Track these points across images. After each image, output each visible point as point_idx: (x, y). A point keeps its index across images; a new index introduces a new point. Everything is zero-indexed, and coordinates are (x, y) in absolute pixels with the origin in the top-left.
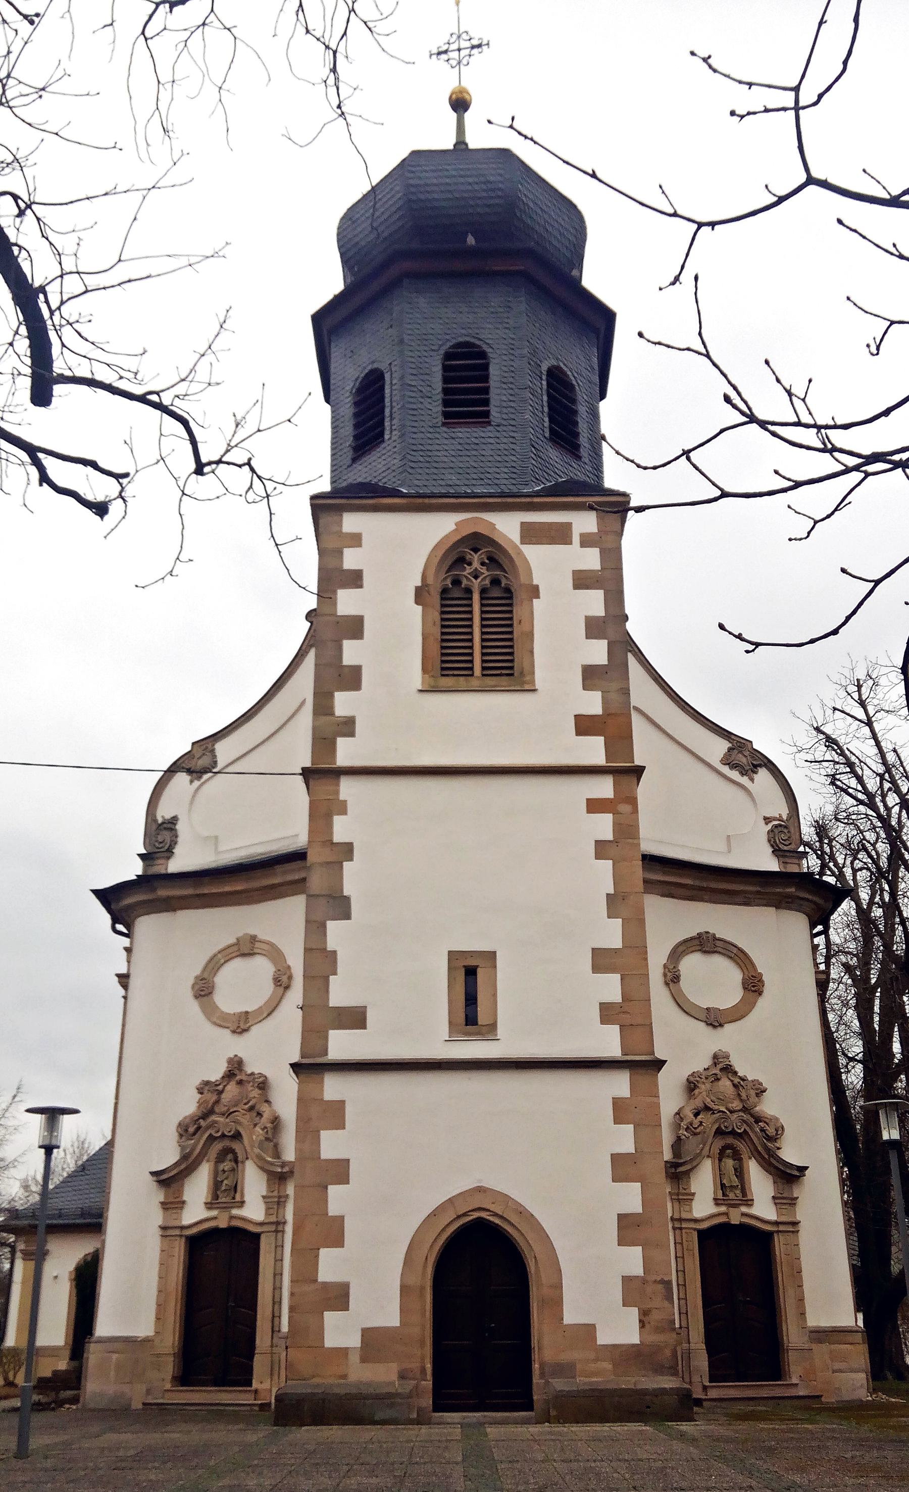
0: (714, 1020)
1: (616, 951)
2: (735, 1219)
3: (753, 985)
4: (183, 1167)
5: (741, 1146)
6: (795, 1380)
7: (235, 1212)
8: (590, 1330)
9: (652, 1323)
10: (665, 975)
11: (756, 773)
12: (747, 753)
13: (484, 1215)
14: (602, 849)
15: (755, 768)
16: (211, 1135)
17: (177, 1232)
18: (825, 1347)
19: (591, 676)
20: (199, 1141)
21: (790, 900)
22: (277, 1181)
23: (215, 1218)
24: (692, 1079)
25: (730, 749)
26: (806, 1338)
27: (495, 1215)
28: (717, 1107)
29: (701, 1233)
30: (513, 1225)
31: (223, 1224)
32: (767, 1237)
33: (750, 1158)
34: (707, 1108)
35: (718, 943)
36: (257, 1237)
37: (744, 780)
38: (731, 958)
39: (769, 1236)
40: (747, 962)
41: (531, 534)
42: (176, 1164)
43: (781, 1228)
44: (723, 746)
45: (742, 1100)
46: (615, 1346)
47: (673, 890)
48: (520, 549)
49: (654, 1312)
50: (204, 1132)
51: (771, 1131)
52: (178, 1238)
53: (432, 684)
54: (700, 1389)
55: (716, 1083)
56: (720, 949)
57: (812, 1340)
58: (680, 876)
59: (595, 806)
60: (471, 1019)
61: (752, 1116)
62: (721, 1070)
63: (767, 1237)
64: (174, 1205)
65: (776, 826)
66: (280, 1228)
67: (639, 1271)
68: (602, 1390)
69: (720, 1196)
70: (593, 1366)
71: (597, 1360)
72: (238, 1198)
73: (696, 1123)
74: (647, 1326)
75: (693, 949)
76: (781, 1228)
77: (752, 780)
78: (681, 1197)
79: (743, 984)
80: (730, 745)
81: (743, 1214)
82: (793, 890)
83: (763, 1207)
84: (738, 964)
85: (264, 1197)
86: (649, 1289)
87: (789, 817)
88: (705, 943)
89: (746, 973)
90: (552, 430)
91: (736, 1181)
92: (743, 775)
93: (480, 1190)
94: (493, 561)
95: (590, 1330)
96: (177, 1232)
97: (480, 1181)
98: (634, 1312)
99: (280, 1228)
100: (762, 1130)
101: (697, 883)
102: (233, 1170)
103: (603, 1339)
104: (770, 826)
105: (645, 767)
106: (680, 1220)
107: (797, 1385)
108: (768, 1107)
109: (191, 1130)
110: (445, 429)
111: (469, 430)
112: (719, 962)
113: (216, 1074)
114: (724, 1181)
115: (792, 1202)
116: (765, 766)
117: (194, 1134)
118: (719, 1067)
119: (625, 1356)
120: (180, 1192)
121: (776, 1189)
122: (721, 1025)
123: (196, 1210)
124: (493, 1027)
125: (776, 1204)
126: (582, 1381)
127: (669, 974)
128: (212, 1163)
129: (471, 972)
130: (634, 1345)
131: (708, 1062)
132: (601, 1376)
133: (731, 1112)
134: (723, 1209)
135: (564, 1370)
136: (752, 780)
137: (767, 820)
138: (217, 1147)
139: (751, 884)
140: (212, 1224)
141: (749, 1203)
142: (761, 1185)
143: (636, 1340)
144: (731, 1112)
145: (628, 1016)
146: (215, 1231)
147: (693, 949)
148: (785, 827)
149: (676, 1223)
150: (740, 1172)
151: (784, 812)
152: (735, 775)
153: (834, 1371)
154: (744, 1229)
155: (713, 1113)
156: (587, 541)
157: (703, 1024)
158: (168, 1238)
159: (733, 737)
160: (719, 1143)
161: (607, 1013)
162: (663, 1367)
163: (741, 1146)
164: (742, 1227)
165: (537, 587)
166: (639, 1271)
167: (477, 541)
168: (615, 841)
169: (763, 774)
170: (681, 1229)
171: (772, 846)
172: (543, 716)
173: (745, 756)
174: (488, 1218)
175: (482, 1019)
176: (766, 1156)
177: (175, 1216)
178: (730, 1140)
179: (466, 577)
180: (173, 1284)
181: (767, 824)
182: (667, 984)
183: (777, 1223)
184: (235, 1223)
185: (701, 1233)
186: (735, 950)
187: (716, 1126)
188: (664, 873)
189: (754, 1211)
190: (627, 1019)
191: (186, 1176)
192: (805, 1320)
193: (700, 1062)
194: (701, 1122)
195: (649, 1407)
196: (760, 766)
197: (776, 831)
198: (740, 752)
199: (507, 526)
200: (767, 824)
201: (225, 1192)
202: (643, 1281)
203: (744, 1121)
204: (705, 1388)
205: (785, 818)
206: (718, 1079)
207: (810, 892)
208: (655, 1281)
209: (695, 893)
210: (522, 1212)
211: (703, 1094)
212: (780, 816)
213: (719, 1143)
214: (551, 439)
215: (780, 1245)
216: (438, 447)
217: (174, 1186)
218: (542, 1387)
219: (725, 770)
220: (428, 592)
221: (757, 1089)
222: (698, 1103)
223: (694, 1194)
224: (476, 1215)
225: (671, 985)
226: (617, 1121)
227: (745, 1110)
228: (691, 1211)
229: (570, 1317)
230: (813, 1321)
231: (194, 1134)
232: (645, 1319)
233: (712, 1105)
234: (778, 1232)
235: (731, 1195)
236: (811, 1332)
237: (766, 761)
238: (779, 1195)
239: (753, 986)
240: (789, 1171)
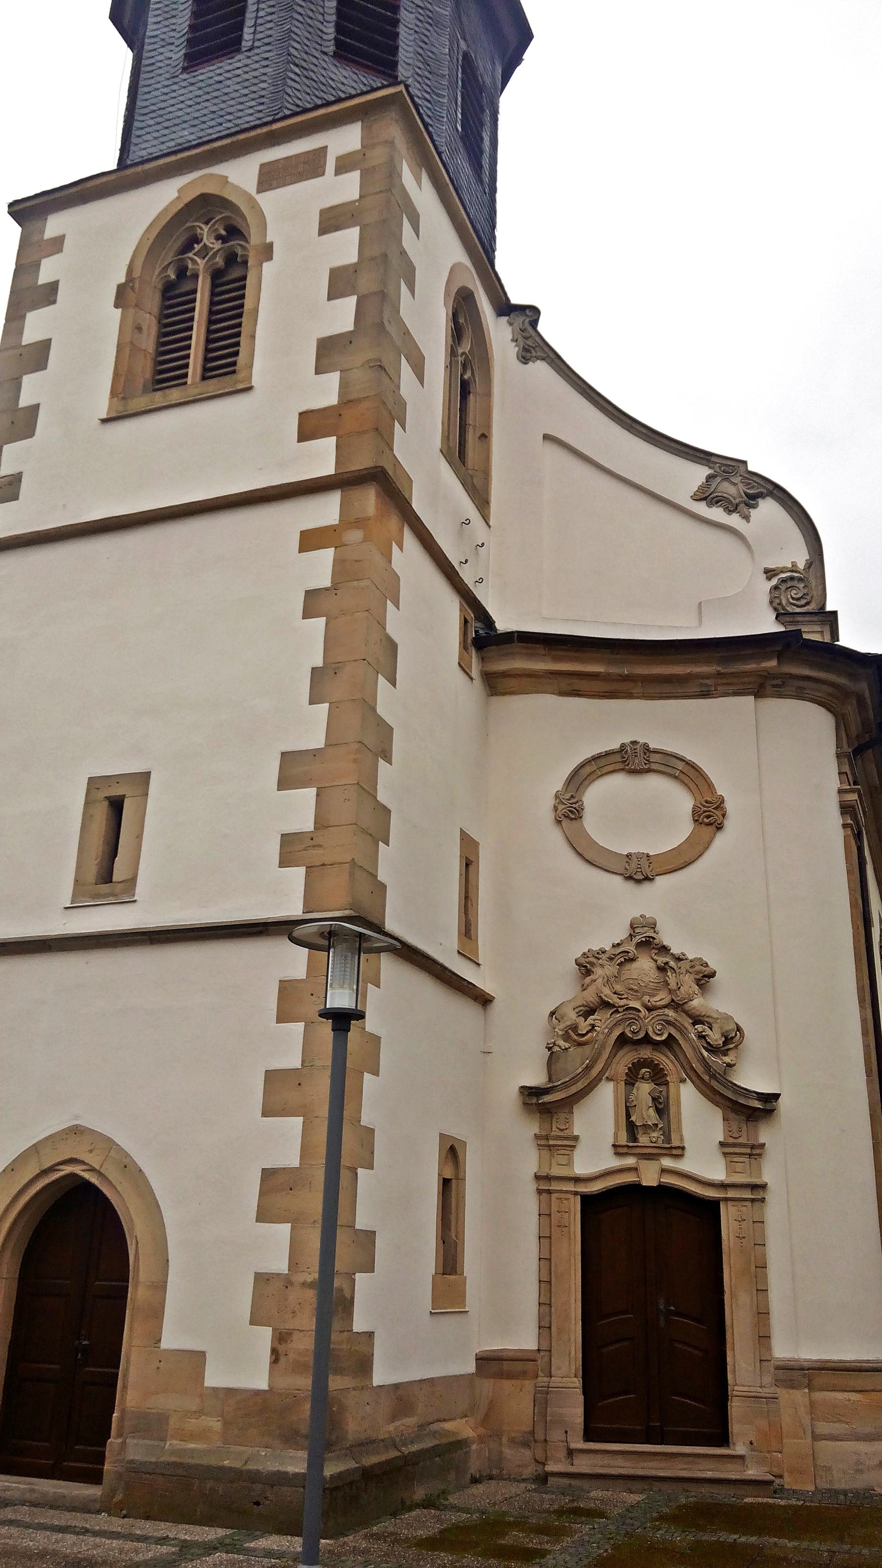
0: (639, 871)
1: (315, 753)
2: (649, 1177)
3: (710, 816)
5: (666, 1061)
6: (740, 1449)
8: (196, 1360)
9: (292, 1356)
10: (556, 809)
11: (754, 507)
12: (737, 480)
13: (77, 1169)
14: (313, 603)
15: (752, 500)
16: (623, 1034)
18: (800, 1396)
19: (329, 352)
21: (779, 682)
24: (583, 961)
25: (709, 478)
26: (768, 1379)
27: (92, 1170)
28: (622, 1003)
29: (587, 1200)
30: (110, 1183)
32: (708, 1210)
33: (683, 1081)
34: (605, 1005)
35: (654, 758)
37: (734, 520)
38: (676, 778)
39: (711, 1208)
40: (700, 781)
41: (270, 178)
43: (731, 1194)
44: (699, 473)
45: (670, 991)
46: (230, 1392)
47: (584, 685)
48: (255, 200)
49: (296, 1336)
51: (715, 1037)
53: (121, 408)
54: (562, 1454)
55: (628, 966)
56: (654, 766)
57: (778, 1382)
58: (582, 661)
59: (310, 540)
60: (106, 876)
61: (687, 1013)
62: (639, 945)
63: (708, 1210)
64: (557, 1144)
65: (784, 581)
67: (282, 1266)
68: (189, 1467)
69: (623, 1139)
70: (192, 1424)
71: (199, 1413)
73: (583, 1026)
74: (283, 1360)
75: (611, 768)
76: (731, 1194)
77: (747, 518)
78: (551, 1142)
79: (694, 812)
80: (710, 471)
81: (664, 1171)
82: (773, 663)
83: (701, 1155)
84: (683, 782)
86: (294, 1296)
87: (809, 565)
88: (634, 760)
89: (699, 797)
90: (338, 43)
91: (652, 1116)
92: (730, 512)
93: (76, 1131)
94: (234, 232)
95: (196, 1360)
96: (570, 1187)
97: (77, 1117)
98: (265, 1335)
100: (701, 1037)
101: (614, 670)
103: (213, 1378)
104: (774, 581)
105: (298, 442)
106: (548, 1178)
107: (742, 1457)
108: (722, 1003)
110: (185, 76)
111: (211, 68)
112: (656, 784)
114: (633, 1118)
115: (756, 1152)
116: (770, 494)
118: (637, 939)
119: (249, 1411)
120: (569, 1121)
121: (728, 1131)
122: (648, 879)
123: (596, 1151)
124: (131, 882)
125: (725, 1154)
126: (173, 1449)
127: (561, 807)
129: (116, 806)
130: (257, 1393)
131: (621, 933)
132: (199, 1441)
133: (649, 1009)
134: (630, 1161)
135: (152, 1425)
136: (747, 518)
137: (770, 573)
139: (708, 662)
141: (678, 1152)
142: (699, 1123)
143: (262, 1384)
144: (649, 1009)
145: (321, 851)
147: (611, 768)
148: (800, 580)
149: (542, 1182)
150: (662, 1107)
151: (801, 557)
152: (717, 514)
153: (816, 1437)
154: (667, 1196)
155: (617, 1012)
156: (344, 165)
157: (618, 879)
159: (713, 459)
160: (626, 1059)
161: (291, 849)
162: (297, 1432)
163: (666, 1061)
164: (663, 1190)
165: (270, 246)
166: (282, 1266)
167: (206, 205)
168: (335, 586)
169: (768, 508)
170: (549, 1192)
171: (775, 609)
172: (260, 424)
173: (735, 484)
174: (83, 1174)
175: (118, 874)
176: (706, 1078)
178: (646, 1053)
179: (192, 259)
181: (769, 579)
182: (559, 822)
183: (723, 1186)
185: (587, 1200)
186: (680, 765)
187: (617, 1033)
188: (556, 659)
189: (685, 1165)
190: (317, 856)
192: (769, 1349)
193: (609, 934)
194: (593, 1026)
195: (257, 1504)
196: (761, 495)
197: (783, 587)
198: (726, 479)
199: (241, 174)
200: (769, 579)
202: (287, 1282)
203: (669, 1023)
204: (571, 1453)
205: (801, 566)
206: (632, 960)
207: (811, 665)
208: (304, 1284)
209: (614, 686)
210: (128, 1166)
211: (600, 984)
212: (794, 564)
213: (626, 1059)
214: (336, 55)
215: (729, 1220)
216: (172, 102)
218: (124, 1449)
219: (701, 509)
220: (133, 288)
221: (698, 973)
222: (590, 996)
223: (576, 1138)
224: (68, 1169)
225: (565, 822)
226: (282, 1017)
227: (674, 1005)
228: (570, 1163)
229: (170, 1340)
230: (782, 1349)
232: (281, 1348)
233: (614, 999)
234: (726, 1200)
235: (643, 1140)
236: (777, 1368)
237: (770, 487)
238: (731, 1140)
239: (708, 817)
240: (742, 1101)
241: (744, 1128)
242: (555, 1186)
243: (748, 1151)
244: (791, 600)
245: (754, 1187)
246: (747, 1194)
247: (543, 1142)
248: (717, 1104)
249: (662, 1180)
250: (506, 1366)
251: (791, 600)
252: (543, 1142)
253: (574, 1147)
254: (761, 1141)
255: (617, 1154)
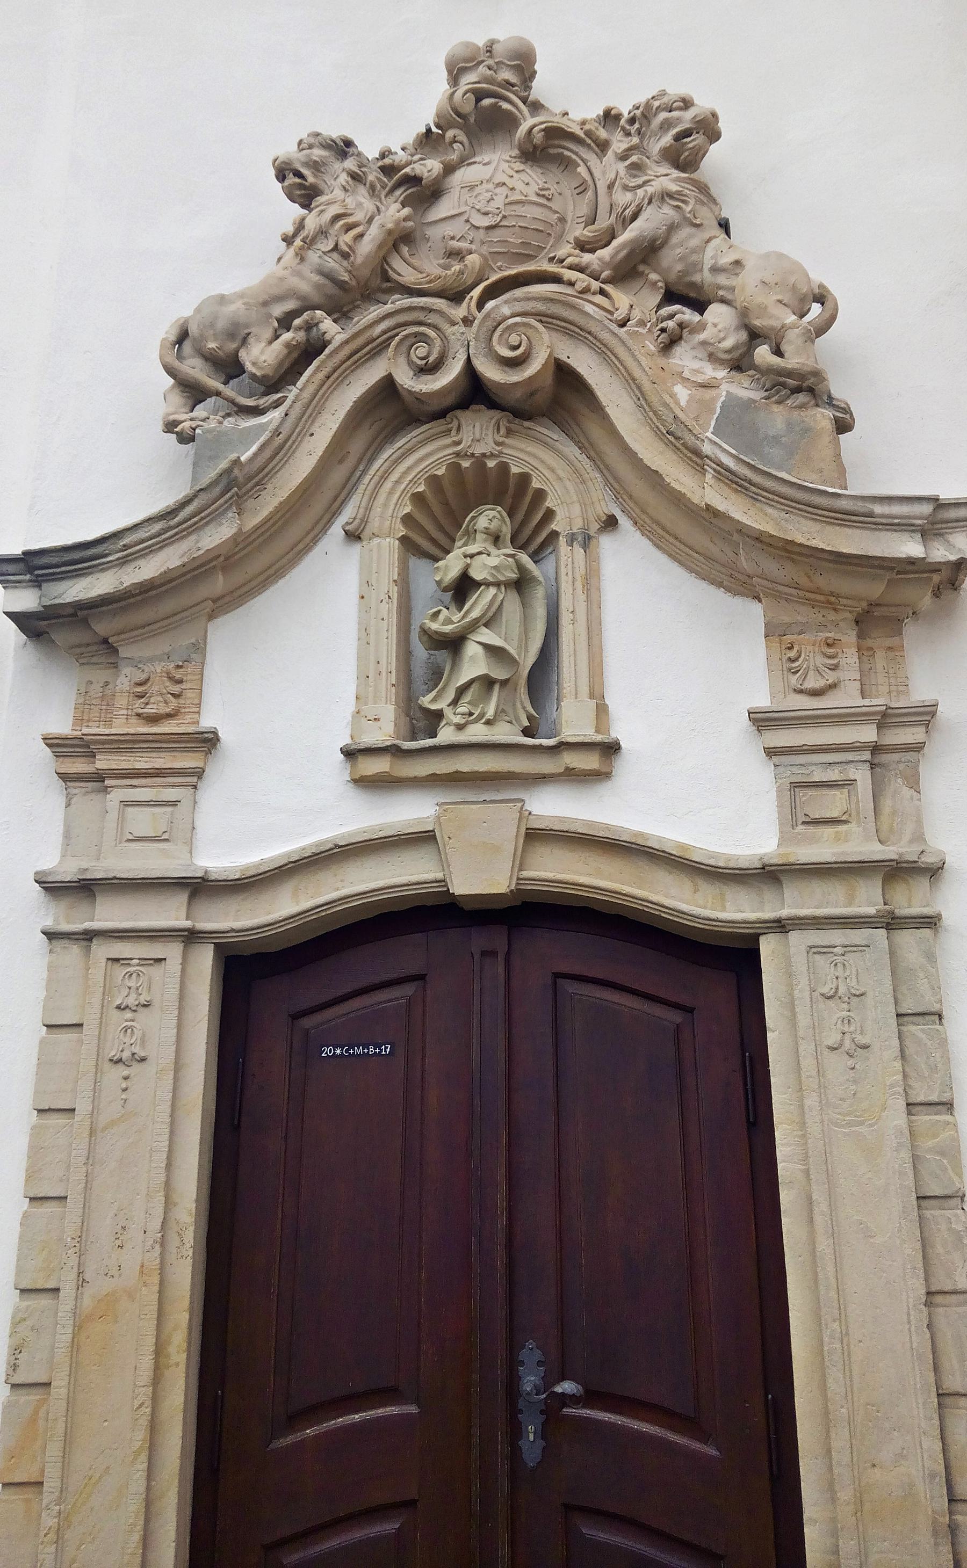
4: (215, 536)
7: (552, 806)
16: (388, 384)
17: (171, 913)
20: (312, 409)
22: (849, 637)
23: (424, 839)
31: (480, 874)
36: (733, 960)
42: (172, 523)
50: (336, 378)
52: (173, 951)
64: (137, 751)
66: (911, 899)
72: (574, 721)
76: (794, 901)
81: (535, 836)
85: (762, 721)
96: (171, 913)
99: (911, 899)
102: (521, 584)
109: (262, 355)
113: (395, 114)
115: (895, 744)
117: (276, 382)
120: (185, 677)
123: (290, 768)
125: (771, 752)
128: (385, 549)
138: (418, 460)
140: (405, 873)
146: (435, 913)
158: (103, 950)
164: (529, 913)
177: (143, 821)
178: (478, 434)
180: (138, 1253)
183: (769, 875)
184: (558, 870)
191: (222, 605)
201: (479, 686)
217: (146, 658)
231: (276, 382)
234: (781, 926)
241: (849, 658)
242: (110, 914)
243: (868, 734)
244: (431, 333)
245: (896, 872)
246: (867, 899)
247: (79, 766)
248: (741, 585)
249: (525, 874)
250: (71, 1400)
251: (431, 333)
252: (79, 766)
253: (199, 773)
254: (920, 693)
255: (363, 783)
